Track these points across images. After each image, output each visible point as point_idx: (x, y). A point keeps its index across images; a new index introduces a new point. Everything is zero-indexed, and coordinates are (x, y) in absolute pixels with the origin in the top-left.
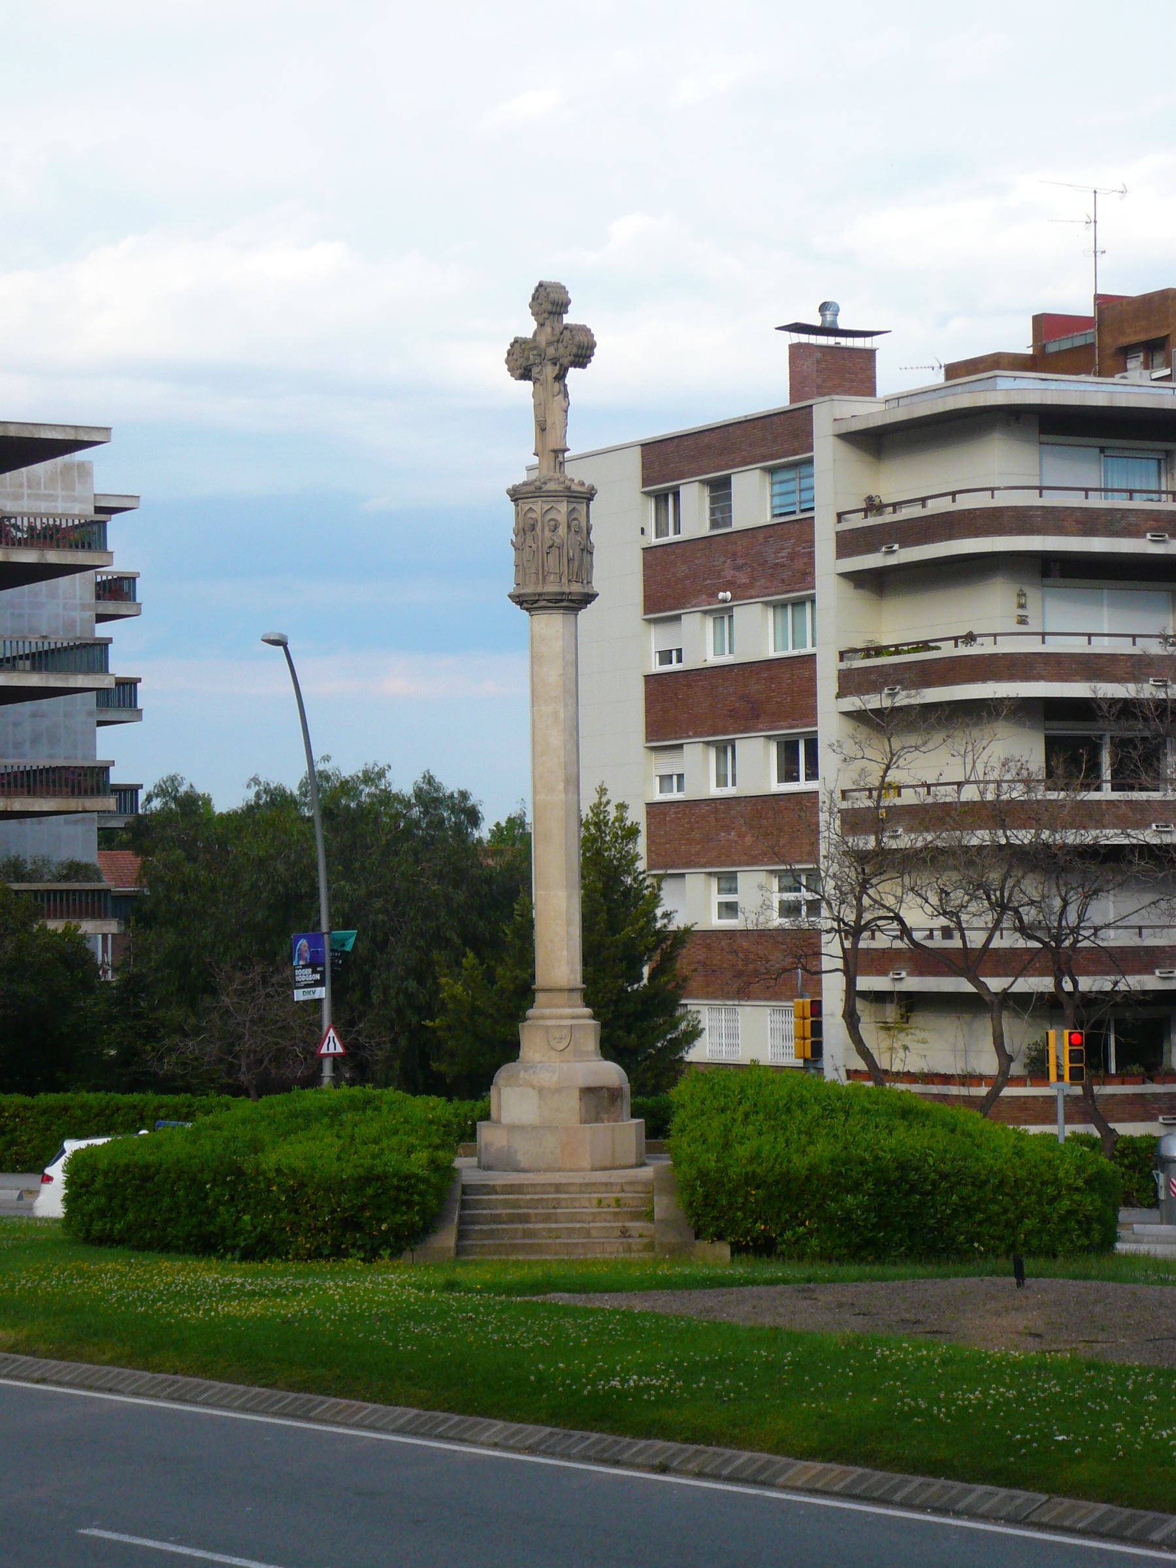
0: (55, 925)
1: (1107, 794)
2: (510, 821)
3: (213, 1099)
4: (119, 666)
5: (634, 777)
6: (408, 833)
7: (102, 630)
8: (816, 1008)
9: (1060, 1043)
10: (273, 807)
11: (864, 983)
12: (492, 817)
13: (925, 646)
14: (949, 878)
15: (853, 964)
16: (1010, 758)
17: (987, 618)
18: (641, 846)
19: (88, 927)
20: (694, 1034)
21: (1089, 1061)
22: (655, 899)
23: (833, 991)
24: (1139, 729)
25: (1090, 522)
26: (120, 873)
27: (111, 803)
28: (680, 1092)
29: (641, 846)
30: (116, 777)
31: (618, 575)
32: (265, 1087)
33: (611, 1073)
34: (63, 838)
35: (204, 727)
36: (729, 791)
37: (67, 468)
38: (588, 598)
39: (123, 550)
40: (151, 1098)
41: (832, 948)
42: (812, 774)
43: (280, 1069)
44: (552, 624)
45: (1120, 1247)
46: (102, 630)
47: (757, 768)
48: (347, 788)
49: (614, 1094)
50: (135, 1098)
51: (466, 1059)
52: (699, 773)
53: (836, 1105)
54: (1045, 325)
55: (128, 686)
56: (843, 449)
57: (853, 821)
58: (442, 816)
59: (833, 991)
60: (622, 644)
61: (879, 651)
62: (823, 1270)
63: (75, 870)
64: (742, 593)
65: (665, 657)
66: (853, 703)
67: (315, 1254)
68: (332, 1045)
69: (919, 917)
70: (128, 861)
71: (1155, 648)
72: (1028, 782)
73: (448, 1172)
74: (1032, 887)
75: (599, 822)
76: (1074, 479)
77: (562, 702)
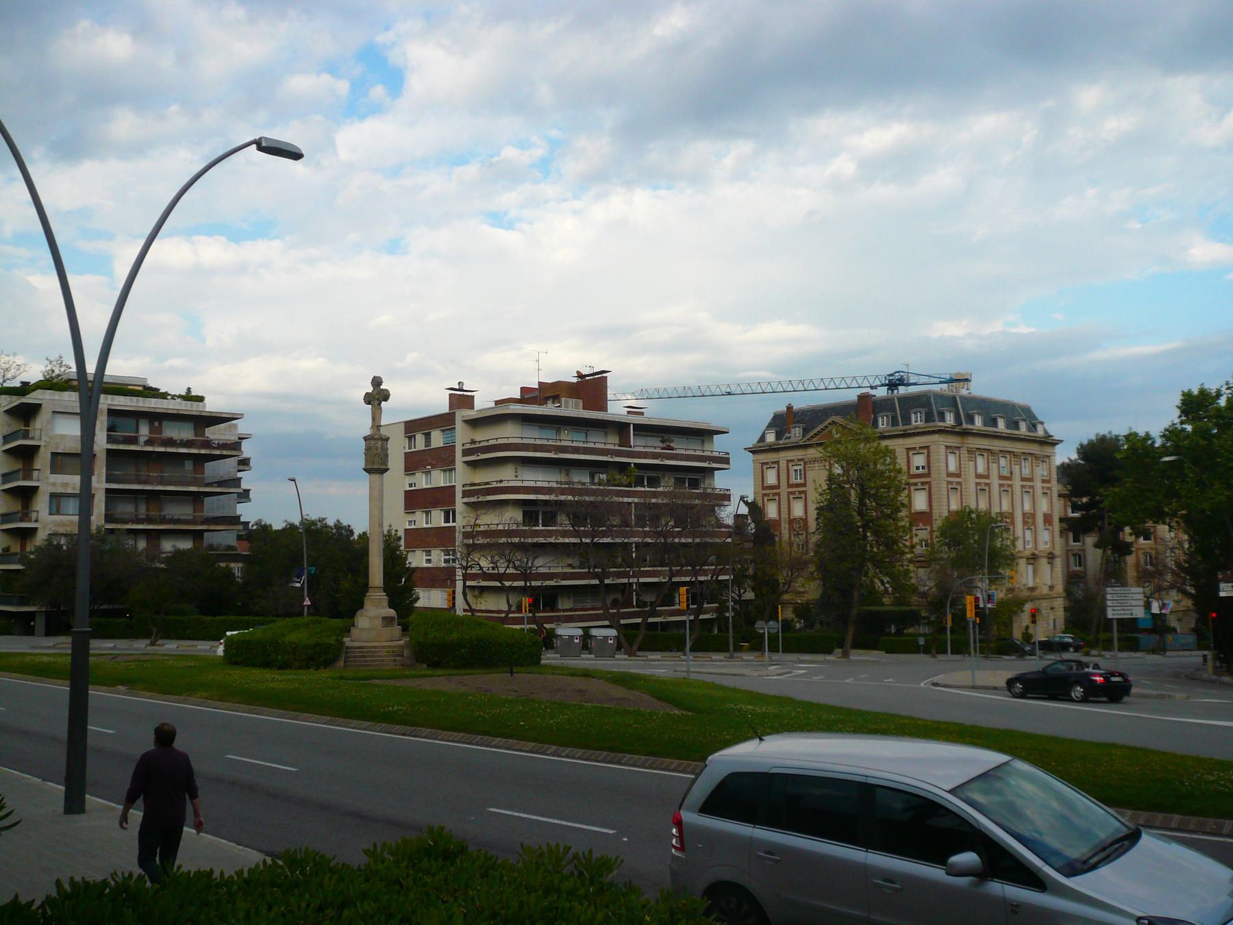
0: (223, 565)
1: (540, 528)
2: (1203, 392)
3: (270, 618)
4: (244, 485)
5: (399, 521)
6: (331, 538)
7: (239, 475)
8: (454, 592)
9: (526, 601)
10: (291, 528)
11: (468, 583)
12: (357, 532)
13: (488, 483)
14: (494, 552)
15: (466, 577)
16: (511, 518)
17: (507, 476)
18: (402, 542)
19: (232, 565)
20: (418, 598)
21: (534, 607)
22: (406, 558)
23: (459, 586)
24: (549, 509)
25: (536, 448)
26: (244, 549)
27: (241, 527)
28: (412, 618)
29: (402, 542)
30: (242, 519)
31: (396, 461)
32: (287, 615)
33: (392, 612)
34: (225, 538)
35: (270, 503)
36: (429, 526)
37: (230, 426)
38: (387, 470)
39: (247, 450)
40: (251, 618)
41: (459, 573)
42: (454, 521)
43: (293, 611)
44: (376, 477)
45: (543, 662)
46: (239, 475)
47: (438, 519)
48: (313, 523)
49: (392, 619)
50: (246, 618)
51: (346, 607)
52: (421, 520)
53: (460, 621)
54: (524, 390)
55: (247, 492)
56: (465, 425)
57: (466, 535)
58: (343, 532)
59: (459, 586)
60: (397, 481)
61: (474, 485)
62: (454, 672)
63: (230, 548)
64: (434, 467)
65: (411, 485)
66: (466, 500)
67: (300, 668)
68: (307, 602)
69: (485, 563)
70: (246, 544)
71: (554, 485)
72: (517, 524)
73: (341, 643)
74: (518, 555)
75: (389, 535)
76: (532, 435)
77: (377, 500)
